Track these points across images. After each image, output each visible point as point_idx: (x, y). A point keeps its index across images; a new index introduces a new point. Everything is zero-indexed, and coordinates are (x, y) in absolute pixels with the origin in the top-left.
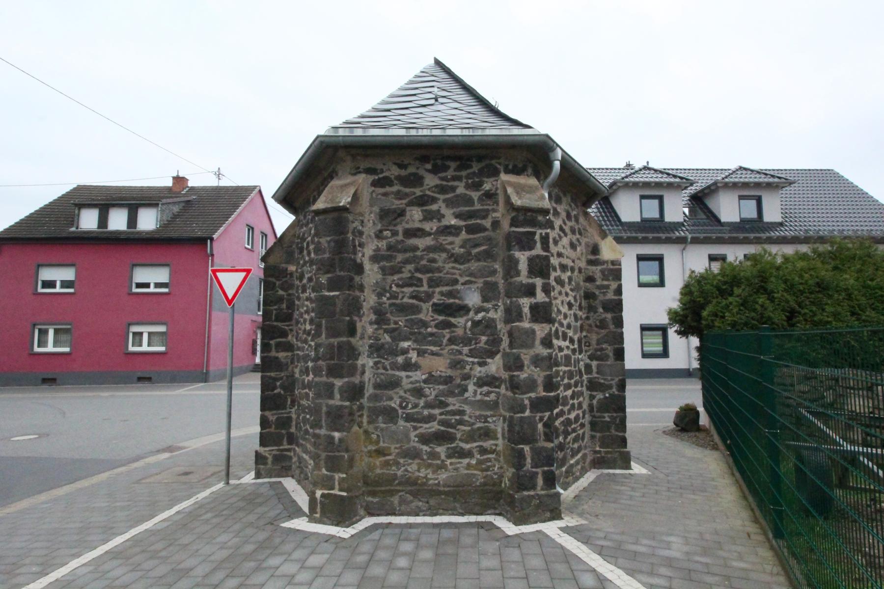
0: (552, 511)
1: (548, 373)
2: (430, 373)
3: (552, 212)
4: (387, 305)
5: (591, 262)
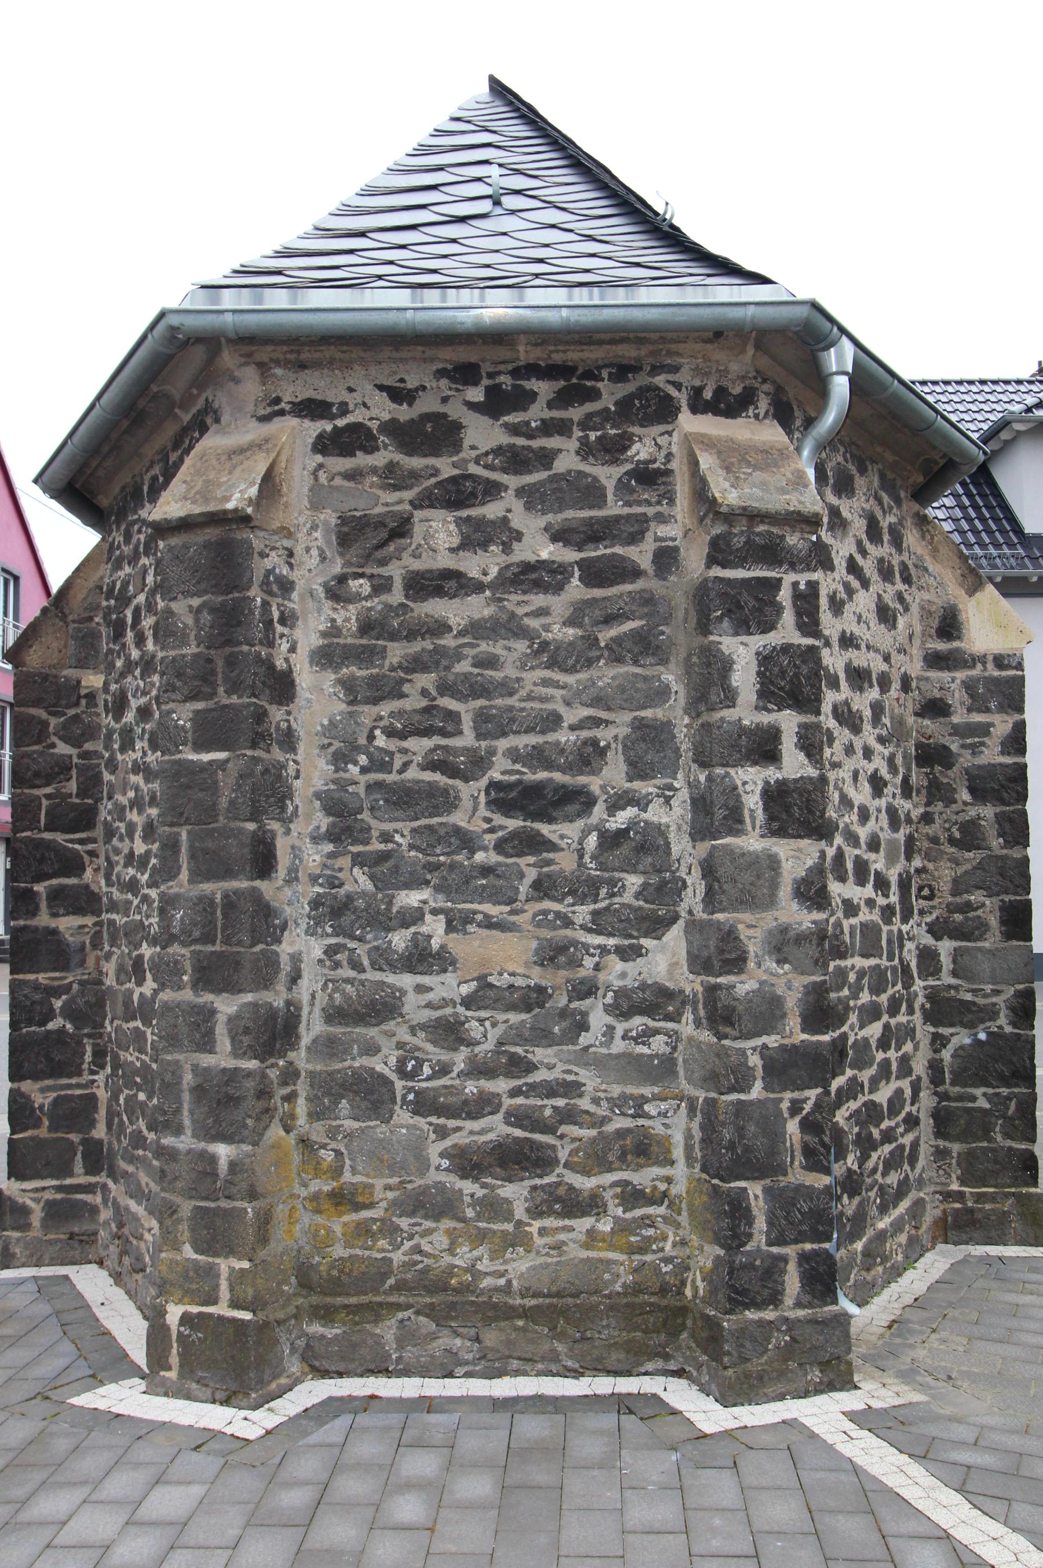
0: (824, 1365)
1: (818, 978)
2: (482, 979)
3: (825, 520)
4: (361, 790)
5: (936, 661)
